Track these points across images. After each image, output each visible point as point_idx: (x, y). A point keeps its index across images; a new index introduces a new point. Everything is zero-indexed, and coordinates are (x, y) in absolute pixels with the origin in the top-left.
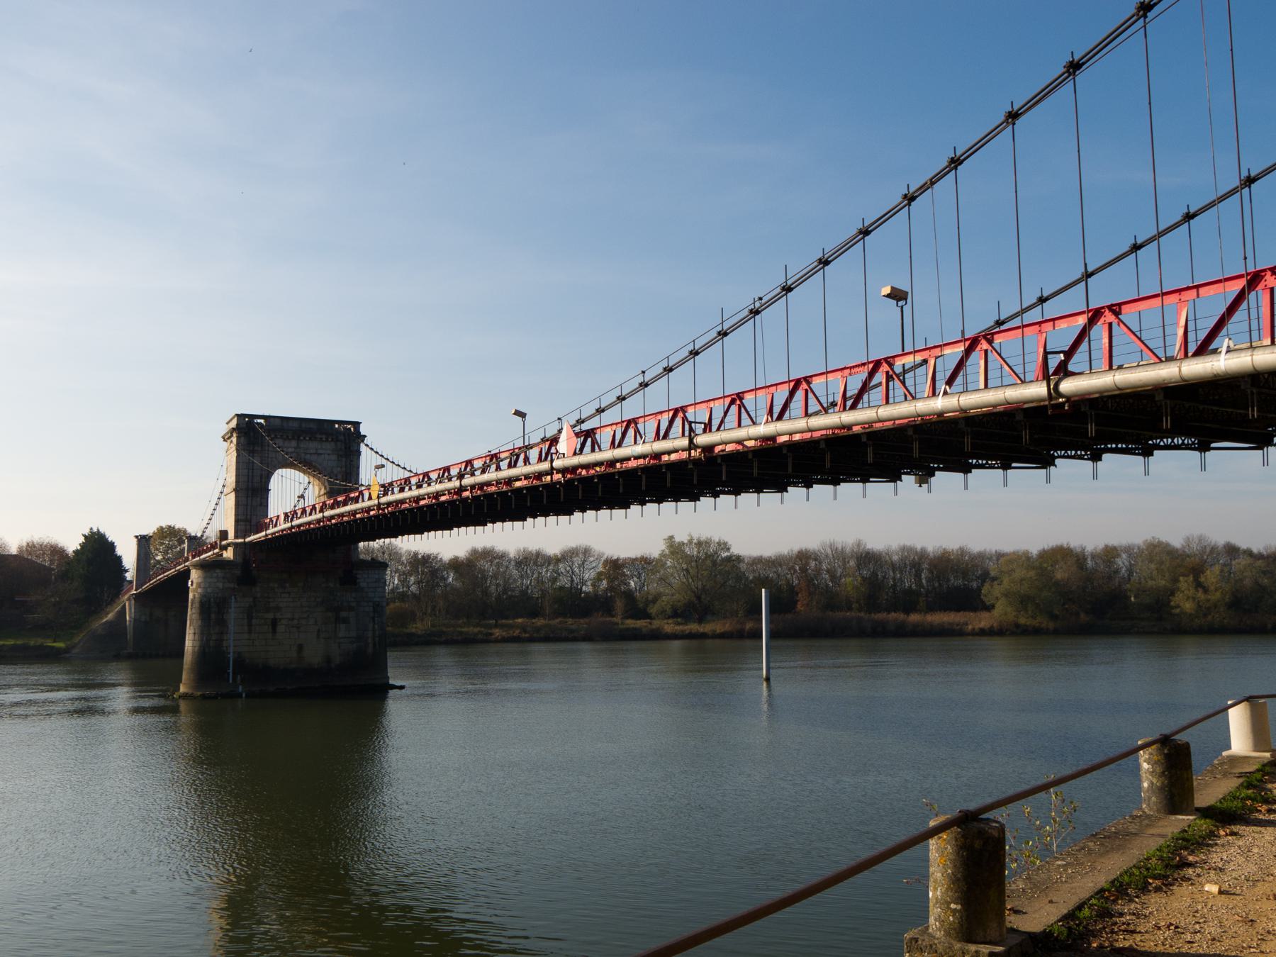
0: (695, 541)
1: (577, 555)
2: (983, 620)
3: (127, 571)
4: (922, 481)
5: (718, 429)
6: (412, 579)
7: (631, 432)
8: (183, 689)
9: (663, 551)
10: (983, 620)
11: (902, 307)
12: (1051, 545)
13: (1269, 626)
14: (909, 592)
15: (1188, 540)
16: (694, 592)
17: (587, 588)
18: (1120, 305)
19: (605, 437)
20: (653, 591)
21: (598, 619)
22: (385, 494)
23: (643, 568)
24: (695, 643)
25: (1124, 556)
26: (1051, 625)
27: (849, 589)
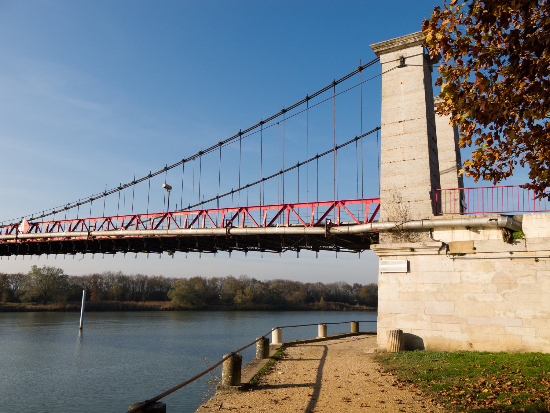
0: (47, 268)
2: (167, 305)
4: (171, 254)
5: (98, 230)
9: (30, 272)
10: (167, 305)
11: (169, 192)
12: (194, 276)
13: (264, 308)
14: (139, 293)
15: (241, 277)
16: (43, 290)
19: (43, 227)
23: (19, 279)
24: (41, 314)
25: (219, 281)
26: (192, 307)
27: (114, 291)
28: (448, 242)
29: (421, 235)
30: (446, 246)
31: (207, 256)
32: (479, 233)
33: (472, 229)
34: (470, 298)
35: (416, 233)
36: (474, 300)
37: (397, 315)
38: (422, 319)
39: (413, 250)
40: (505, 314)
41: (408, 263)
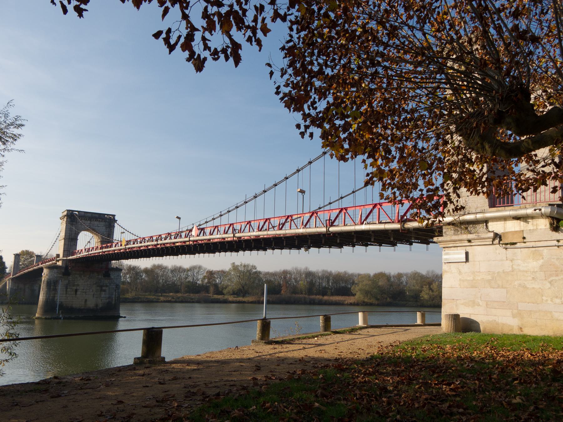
1: (196, 269)
2: (351, 300)
3: (6, 268)
4: (306, 250)
6: (128, 276)
7: (216, 230)
8: (37, 315)
10: (351, 300)
14: (325, 288)
17: (199, 282)
18: (347, 208)
19: (208, 231)
20: (225, 284)
21: (203, 295)
22: (127, 244)
24: (241, 305)
25: (405, 277)
26: (376, 302)
28: (501, 232)
29: (478, 227)
30: (498, 236)
31: (386, 249)
32: (528, 223)
33: (522, 219)
34: (520, 285)
35: (474, 225)
36: (525, 287)
37: (458, 301)
38: (479, 305)
39: (469, 241)
40: (552, 301)
41: (467, 254)
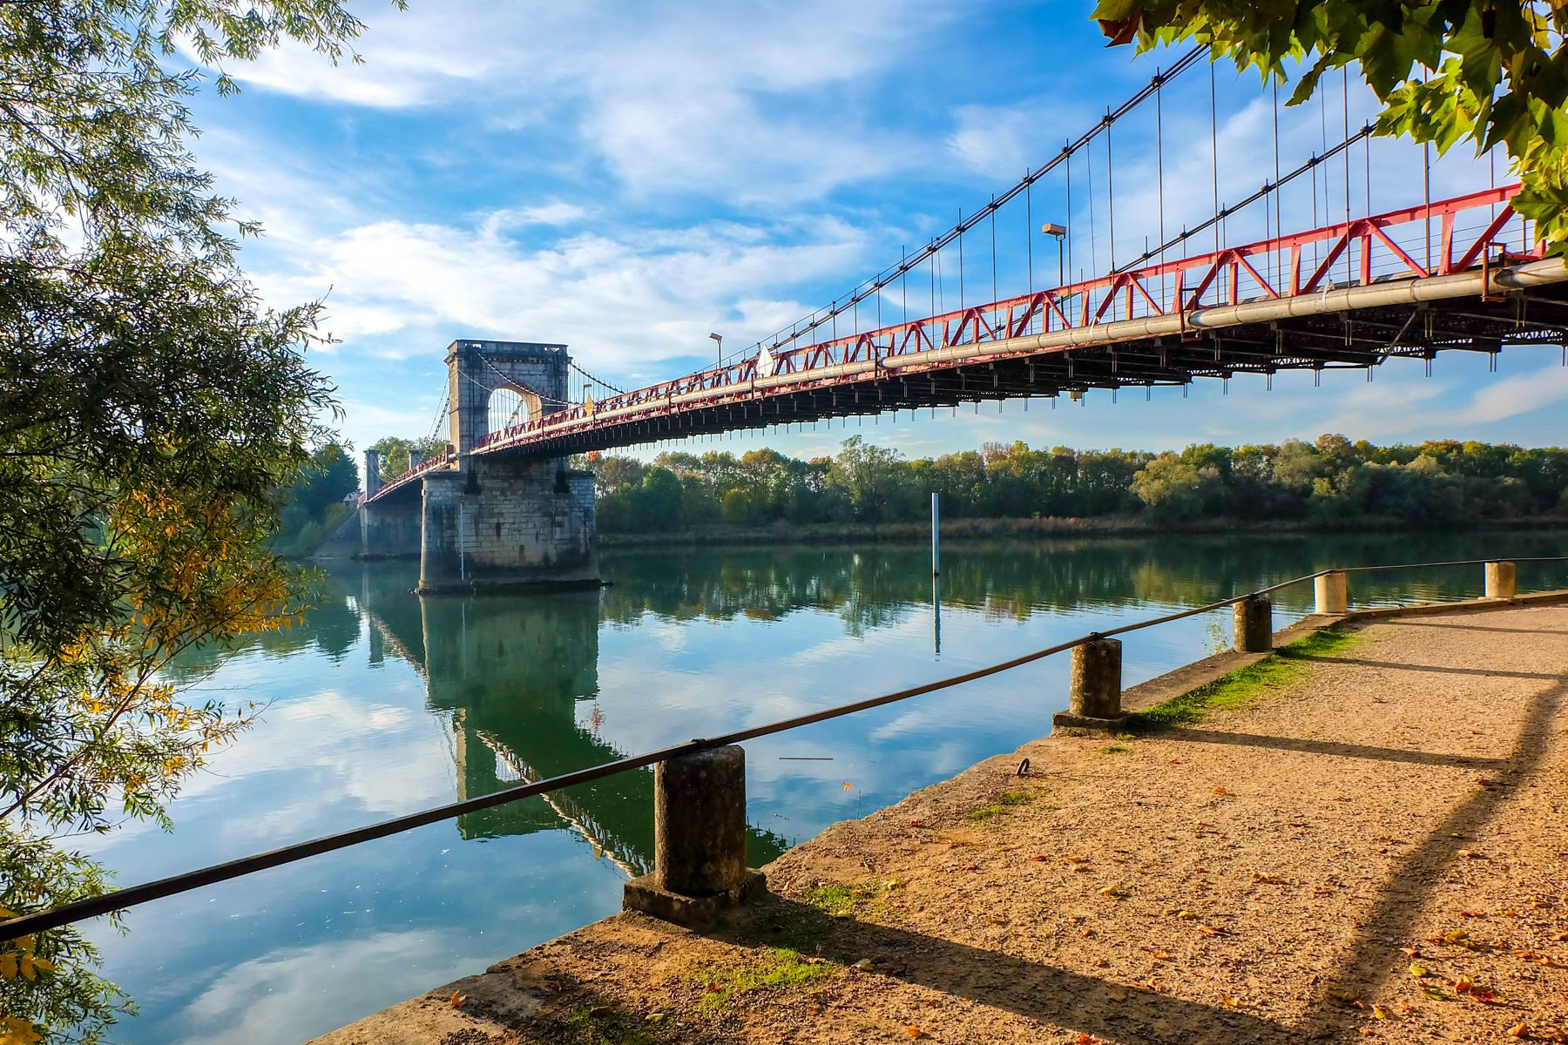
5: (900, 353)
